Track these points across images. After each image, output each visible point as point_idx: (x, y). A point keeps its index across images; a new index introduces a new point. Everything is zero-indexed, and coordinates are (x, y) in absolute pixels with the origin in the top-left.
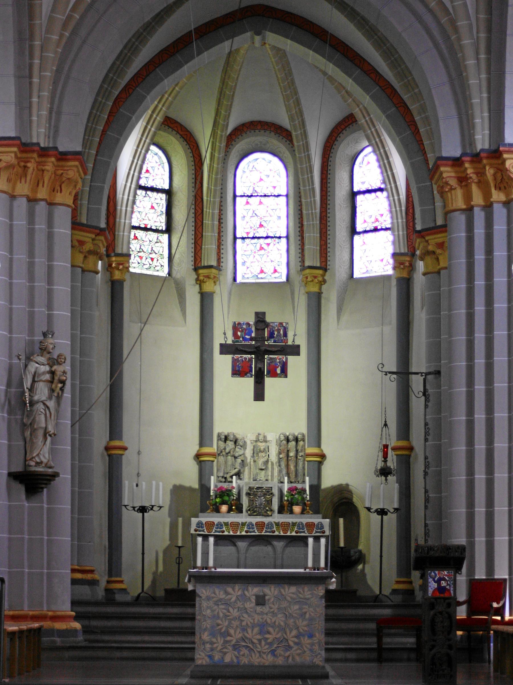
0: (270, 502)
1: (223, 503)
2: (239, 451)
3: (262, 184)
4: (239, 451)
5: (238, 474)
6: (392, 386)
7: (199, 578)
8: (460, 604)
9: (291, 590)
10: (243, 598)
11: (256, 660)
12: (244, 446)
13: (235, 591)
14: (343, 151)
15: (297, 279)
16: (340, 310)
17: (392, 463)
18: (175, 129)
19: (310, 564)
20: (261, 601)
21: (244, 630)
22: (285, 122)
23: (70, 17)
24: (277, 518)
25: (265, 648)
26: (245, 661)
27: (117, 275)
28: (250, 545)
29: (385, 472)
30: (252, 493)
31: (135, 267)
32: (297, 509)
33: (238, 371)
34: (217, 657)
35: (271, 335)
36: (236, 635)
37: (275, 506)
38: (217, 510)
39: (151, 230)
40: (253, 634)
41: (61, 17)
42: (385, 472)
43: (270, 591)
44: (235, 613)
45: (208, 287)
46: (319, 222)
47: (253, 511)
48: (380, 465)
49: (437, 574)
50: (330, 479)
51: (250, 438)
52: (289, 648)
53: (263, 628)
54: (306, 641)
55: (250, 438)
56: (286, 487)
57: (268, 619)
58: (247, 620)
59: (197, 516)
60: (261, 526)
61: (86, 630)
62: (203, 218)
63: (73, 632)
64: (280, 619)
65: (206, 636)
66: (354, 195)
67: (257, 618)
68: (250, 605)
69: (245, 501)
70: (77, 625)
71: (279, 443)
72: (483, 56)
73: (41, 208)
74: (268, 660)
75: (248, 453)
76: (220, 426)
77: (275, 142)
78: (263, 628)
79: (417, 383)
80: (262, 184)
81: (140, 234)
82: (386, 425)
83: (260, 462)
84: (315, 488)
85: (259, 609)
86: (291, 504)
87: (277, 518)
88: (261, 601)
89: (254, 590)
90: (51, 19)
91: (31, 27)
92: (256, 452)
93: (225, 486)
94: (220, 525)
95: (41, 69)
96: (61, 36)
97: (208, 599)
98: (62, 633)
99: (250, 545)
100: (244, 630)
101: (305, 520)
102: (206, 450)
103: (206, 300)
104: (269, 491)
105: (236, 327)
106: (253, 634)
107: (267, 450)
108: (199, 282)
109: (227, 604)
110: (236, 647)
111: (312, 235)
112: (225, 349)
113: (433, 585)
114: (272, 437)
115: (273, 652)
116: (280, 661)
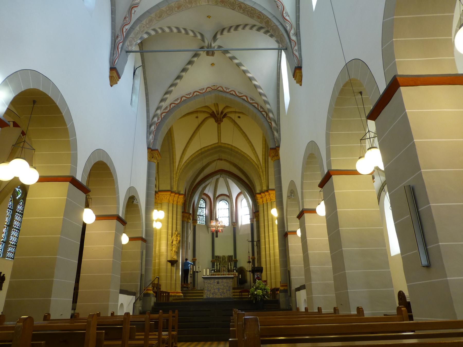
6: (250, 244)
9: (225, 280)
13: (212, 281)
17: (251, 260)
20: (218, 283)
21: (214, 289)
22: (228, 194)
25: (219, 294)
26: (215, 297)
29: (249, 262)
36: (213, 291)
40: (216, 291)
42: (249, 262)
43: (220, 281)
44: (212, 286)
49: (257, 274)
52: (224, 294)
53: (219, 289)
54: (228, 292)
58: (215, 287)
61: (184, 296)
63: (181, 296)
64: (222, 287)
67: (217, 287)
68: (216, 284)
72: (264, 173)
73: (239, 294)
74: (220, 297)
78: (219, 289)
79: (255, 243)
88: (218, 283)
89: (216, 281)
92: (223, 260)
95: (176, 178)
98: (178, 296)
100: (214, 289)
106: (216, 291)
109: (210, 284)
110: (213, 294)
116: (222, 297)
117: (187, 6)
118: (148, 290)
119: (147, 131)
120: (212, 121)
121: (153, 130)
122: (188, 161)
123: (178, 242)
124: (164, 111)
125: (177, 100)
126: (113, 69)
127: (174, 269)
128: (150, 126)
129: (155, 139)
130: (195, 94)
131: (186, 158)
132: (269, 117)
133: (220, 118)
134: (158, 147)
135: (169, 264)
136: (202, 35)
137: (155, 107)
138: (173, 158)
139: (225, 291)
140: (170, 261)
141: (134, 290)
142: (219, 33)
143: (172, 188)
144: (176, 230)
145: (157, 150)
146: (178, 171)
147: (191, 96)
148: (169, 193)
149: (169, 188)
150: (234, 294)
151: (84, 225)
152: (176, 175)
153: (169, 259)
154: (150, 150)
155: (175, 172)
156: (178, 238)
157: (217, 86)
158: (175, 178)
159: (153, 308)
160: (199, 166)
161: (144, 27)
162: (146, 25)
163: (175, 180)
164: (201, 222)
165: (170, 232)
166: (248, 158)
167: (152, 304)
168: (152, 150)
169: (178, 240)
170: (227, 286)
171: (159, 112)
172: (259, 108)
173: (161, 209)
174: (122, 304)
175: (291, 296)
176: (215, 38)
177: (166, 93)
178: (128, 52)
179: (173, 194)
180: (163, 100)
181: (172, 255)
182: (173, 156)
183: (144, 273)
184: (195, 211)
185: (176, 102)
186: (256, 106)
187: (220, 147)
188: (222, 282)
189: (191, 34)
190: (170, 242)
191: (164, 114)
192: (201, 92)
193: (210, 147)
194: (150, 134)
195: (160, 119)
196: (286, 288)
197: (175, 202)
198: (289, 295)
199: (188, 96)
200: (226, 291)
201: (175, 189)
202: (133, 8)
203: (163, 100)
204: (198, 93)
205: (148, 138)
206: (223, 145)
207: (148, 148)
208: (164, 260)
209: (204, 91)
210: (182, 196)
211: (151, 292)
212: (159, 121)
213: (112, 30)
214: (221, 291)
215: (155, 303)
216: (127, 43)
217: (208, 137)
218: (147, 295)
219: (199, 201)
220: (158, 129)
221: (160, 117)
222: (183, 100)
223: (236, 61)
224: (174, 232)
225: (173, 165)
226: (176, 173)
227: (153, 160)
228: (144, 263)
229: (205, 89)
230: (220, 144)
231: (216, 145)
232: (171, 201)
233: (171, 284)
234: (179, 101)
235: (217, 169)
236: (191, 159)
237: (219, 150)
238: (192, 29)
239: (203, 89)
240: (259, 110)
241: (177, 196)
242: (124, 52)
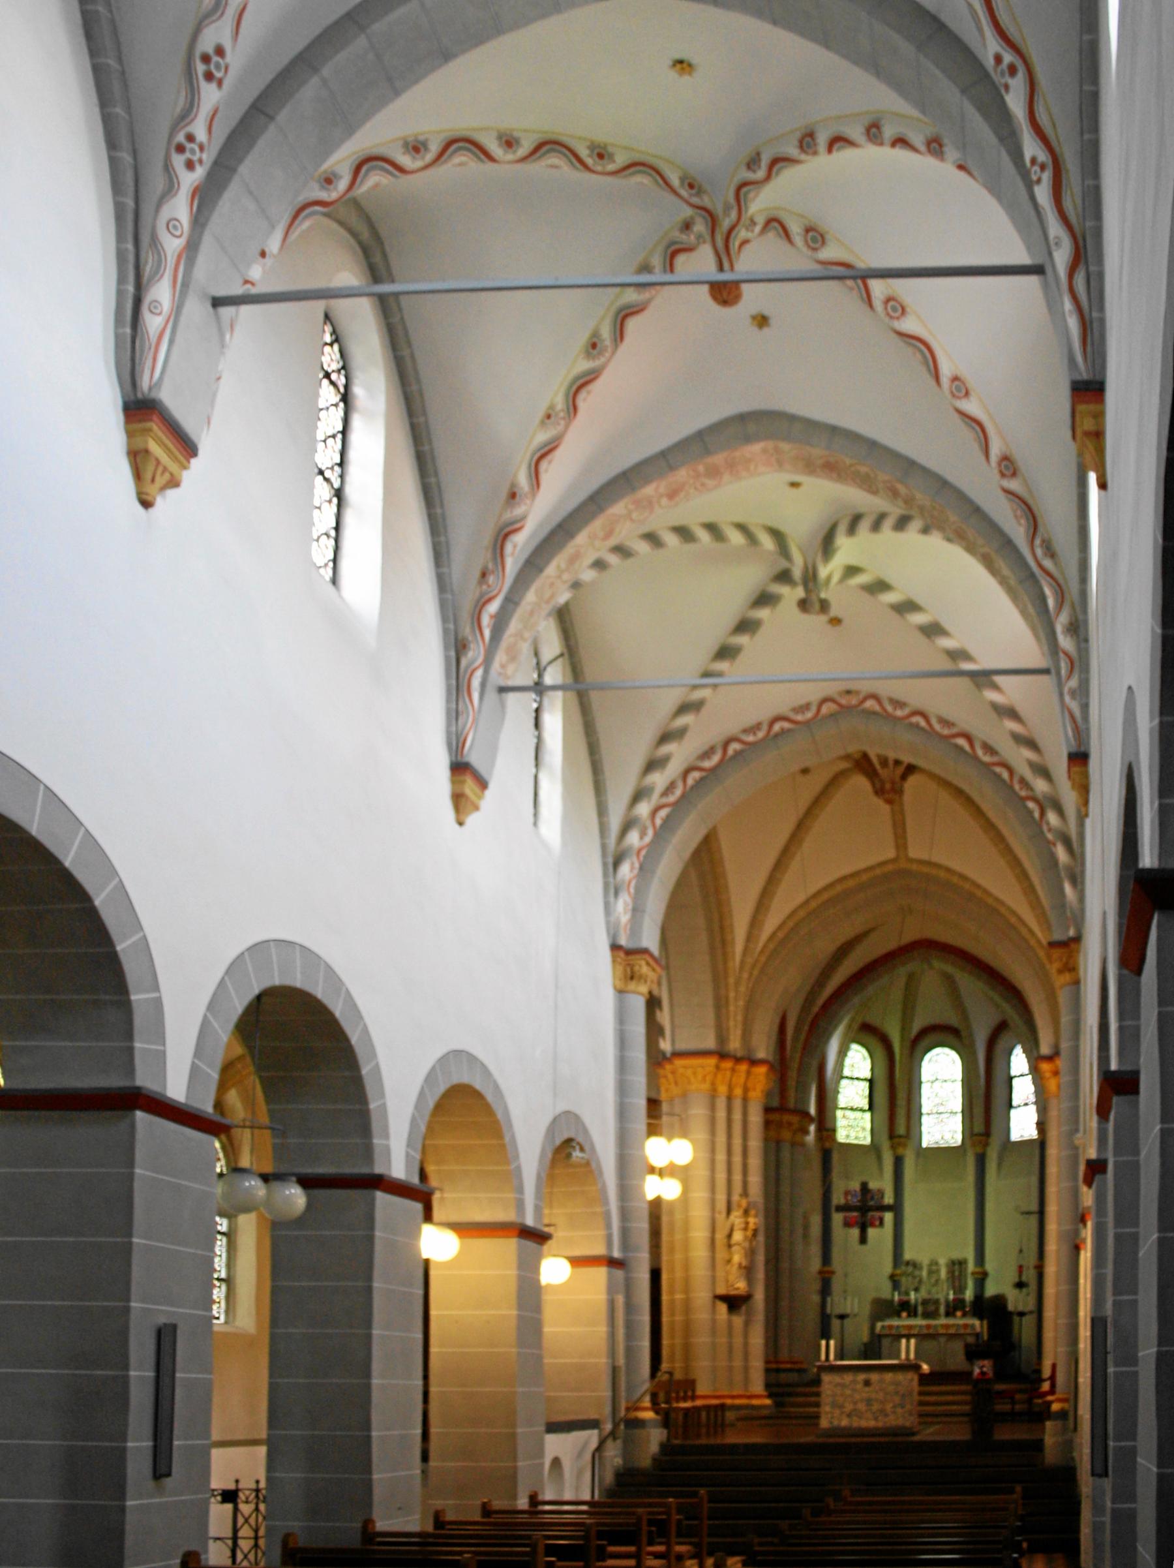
0: (937, 1309)
1: (903, 1310)
2: (917, 1273)
3: (942, 1074)
4: (917, 1273)
5: (916, 1290)
7: (822, 1369)
8: (1045, 1380)
9: (889, 1376)
10: (854, 1382)
11: (864, 1424)
12: (921, 1268)
13: (848, 1378)
14: (1001, 1045)
15: (968, 1142)
16: (999, 1165)
18: (869, 1033)
19: (903, 1356)
21: (855, 1403)
23: (757, 961)
24: (943, 1321)
25: (869, 1415)
27: (827, 1145)
28: (948, 1340)
30: (925, 1302)
31: (842, 1136)
32: (959, 1314)
33: (847, 1224)
34: (836, 1423)
35: (872, 1198)
36: (849, 1407)
37: (942, 1310)
38: (899, 1316)
39: (856, 1110)
40: (862, 1406)
41: (750, 960)
43: (874, 1377)
44: (848, 1392)
45: (900, 1151)
46: (985, 1099)
47: (926, 1315)
48: (1017, 1280)
49: (981, 1363)
50: (991, 1290)
51: (925, 1262)
52: (886, 1415)
53: (869, 1402)
54: (899, 1410)
55: (925, 1262)
56: (951, 1297)
57: (873, 1396)
58: (857, 1397)
59: (882, 1320)
60: (928, 1327)
61: (778, 1405)
62: (896, 1098)
64: (881, 1396)
65: (827, 1409)
66: (1011, 1078)
68: (859, 1386)
69: (920, 1309)
70: (768, 1402)
71: (947, 1265)
74: (872, 1423)
75: (924, 1273)
76: (907, 1256)
77: (951, 1038)
78: (869, 1402)
80: (942, 1074)
81: (848, 1113)
82: (1021, 1251)
83: (933, 1280)
84: (979, 1297)
85: (867, 1389)
86: (955, 1309)
87: (943, 1321)
89: (861, 1377)
90: (742, 962)
91: (726, 970)
92: (930, 1272)
93: (905, 1298)
94: (898, 1327)
95: (736, 999)
96: (751, 974)
97: (830, 1382)
99: (948, 1340)
100: (855, 1403)
101: (961, 1322)
102: (898, 1272)
103: (898, 1162)
104: (937, 1302)
105: (847, 1193)
106: (862, 1406)
107: (938, 1271)
108: (893, 1147)
109: (843, 1386)
110: (849, 1416)
111: (979, 1110)
112: (839, 1209)
113: (977, 1371)
114: (942, 1261)
115: (876, 1419)
116: (880, 1424)
117: (703, 485)
118: (637, 1409)
119: (606, 886)
120: (860, 782)
121: (627, 878)
122: (780, 935)
123: (749, 1233)
124: (664, 800)
125: (707, 754)
126: (460, 768)
127: (738, 1321)
128: (616, 864)
129: (637, 910)
130: (777, 727)
131: (771, 923)
132: (1048, 823)
133: (893, 783)
134: (650, 940)
135: (723, 1308)
136: (777, 535)
137: (637, 762)
138: (722, 928)
139: (889, 1407)
140: (724, 1298)
141: (593, 1415)
142: (842, 529)
143: (722, 1038)
144: (745, 1193)
145: (645, 951)
146: (745, 975)
147: (760, 735)
148: (712, 1061)
149: (710, 1043)
150: (920, 1408)
151: (427, 1262)
152: (737, 991)
153: (721, 1290)
154: (622, 954)
155: (731, 980)
156: (752, 1220)
157: (857, 693)
158: (731, 1000)
159: (654, 1459)
160: (825, 946)
161: (552, 585)
162: (559, 577)
163: (732, 1008)
164: (853, 1134)
165: (721, 1197)
166: (1013, 920)
167: (654, 1448)
168: (629, 952)
169: (751, 1226)
170: (897, 1393)
171: (643, 809)
172: (1017, 787)
173: (684, 1134)
174: (556, 1462)
175: (1075, 1429)
176: (827, 545)
177: (665, 737)
178: (503, 690)
179: (728, 1064)
180: (652, 765)
181: (731, 1278)
182: (721, 919)
183: (621, 1361)
184: (829, 1095)
185: (707, 764)
186: (1005, 775)
187: (902, 873)
188: (881, 1381)
189: (736, 538)
190: (720, 1236)
191: (663, 813)
192: (799, 718)
193: (864, 877)
194: (616, 894)
195: (650, 833)
196: (1066, 1406)
197: (738, 1092)
198: (1071, 1426)
199: (750, 738)
200: (894, 1407)
201: (735, 1044)
202: (506, 536)
203: (652, 765)
204: (786, 725)
205: (608, 909)
206: (914, 867)
207: (615, 947)
208: (702, 1296)
209: (809, 715)
210: (762, 1070)
211: (649, 1415)
212: (648, 838)
213: (444, 619)
214: (876, 1407)
215: (665, 1448)
216: (500, 657)
217: (850, 842)
218: (639, 1424)
219: (843, 1053)
220: (645, 871)
221: (648, 823)
222: (730, 752)
223: (918, 619)
224: (736, 1198)
225: (725, 954)
226: (737, 983)
227: (632, 986)
228: (621, 1332)
229: (814, 709)
230: (903, 864)
231: (890, 867)
232: (723, 1089)
233: (730, 1369)
234: (716, 758)
235: (907, 938)
236: (791, 924)
237: (902, 879)
238: (739, 519)
239: (807, 706)
240: (1015, 793)
241: (743, 1067)
242: (491, 695)
